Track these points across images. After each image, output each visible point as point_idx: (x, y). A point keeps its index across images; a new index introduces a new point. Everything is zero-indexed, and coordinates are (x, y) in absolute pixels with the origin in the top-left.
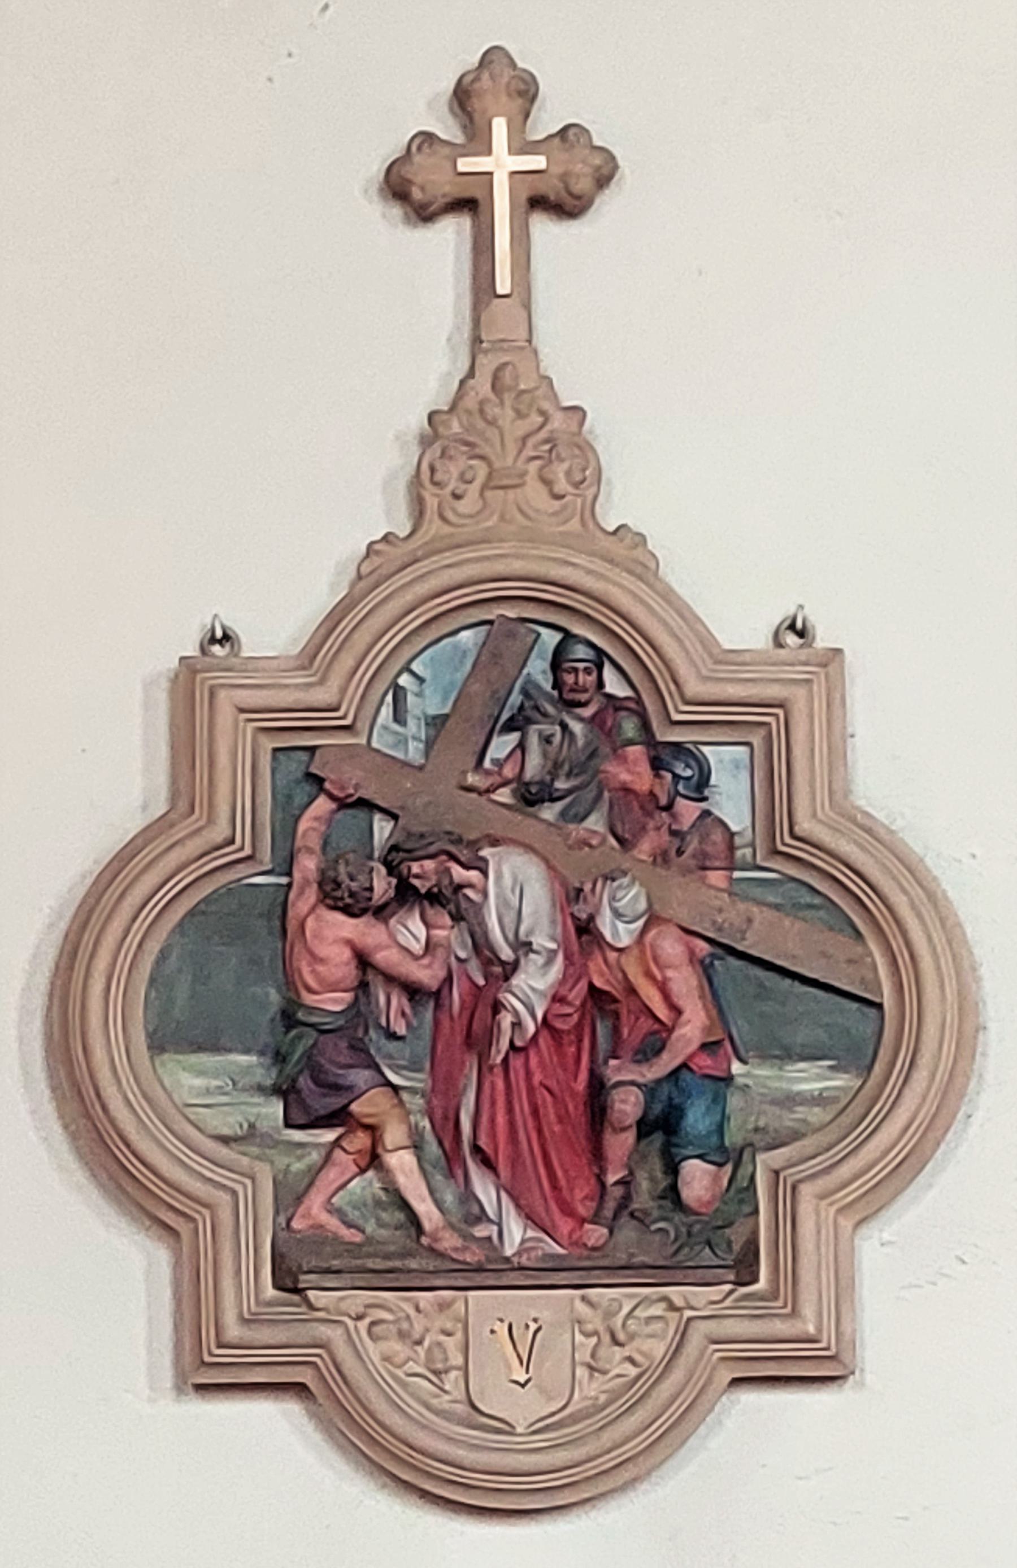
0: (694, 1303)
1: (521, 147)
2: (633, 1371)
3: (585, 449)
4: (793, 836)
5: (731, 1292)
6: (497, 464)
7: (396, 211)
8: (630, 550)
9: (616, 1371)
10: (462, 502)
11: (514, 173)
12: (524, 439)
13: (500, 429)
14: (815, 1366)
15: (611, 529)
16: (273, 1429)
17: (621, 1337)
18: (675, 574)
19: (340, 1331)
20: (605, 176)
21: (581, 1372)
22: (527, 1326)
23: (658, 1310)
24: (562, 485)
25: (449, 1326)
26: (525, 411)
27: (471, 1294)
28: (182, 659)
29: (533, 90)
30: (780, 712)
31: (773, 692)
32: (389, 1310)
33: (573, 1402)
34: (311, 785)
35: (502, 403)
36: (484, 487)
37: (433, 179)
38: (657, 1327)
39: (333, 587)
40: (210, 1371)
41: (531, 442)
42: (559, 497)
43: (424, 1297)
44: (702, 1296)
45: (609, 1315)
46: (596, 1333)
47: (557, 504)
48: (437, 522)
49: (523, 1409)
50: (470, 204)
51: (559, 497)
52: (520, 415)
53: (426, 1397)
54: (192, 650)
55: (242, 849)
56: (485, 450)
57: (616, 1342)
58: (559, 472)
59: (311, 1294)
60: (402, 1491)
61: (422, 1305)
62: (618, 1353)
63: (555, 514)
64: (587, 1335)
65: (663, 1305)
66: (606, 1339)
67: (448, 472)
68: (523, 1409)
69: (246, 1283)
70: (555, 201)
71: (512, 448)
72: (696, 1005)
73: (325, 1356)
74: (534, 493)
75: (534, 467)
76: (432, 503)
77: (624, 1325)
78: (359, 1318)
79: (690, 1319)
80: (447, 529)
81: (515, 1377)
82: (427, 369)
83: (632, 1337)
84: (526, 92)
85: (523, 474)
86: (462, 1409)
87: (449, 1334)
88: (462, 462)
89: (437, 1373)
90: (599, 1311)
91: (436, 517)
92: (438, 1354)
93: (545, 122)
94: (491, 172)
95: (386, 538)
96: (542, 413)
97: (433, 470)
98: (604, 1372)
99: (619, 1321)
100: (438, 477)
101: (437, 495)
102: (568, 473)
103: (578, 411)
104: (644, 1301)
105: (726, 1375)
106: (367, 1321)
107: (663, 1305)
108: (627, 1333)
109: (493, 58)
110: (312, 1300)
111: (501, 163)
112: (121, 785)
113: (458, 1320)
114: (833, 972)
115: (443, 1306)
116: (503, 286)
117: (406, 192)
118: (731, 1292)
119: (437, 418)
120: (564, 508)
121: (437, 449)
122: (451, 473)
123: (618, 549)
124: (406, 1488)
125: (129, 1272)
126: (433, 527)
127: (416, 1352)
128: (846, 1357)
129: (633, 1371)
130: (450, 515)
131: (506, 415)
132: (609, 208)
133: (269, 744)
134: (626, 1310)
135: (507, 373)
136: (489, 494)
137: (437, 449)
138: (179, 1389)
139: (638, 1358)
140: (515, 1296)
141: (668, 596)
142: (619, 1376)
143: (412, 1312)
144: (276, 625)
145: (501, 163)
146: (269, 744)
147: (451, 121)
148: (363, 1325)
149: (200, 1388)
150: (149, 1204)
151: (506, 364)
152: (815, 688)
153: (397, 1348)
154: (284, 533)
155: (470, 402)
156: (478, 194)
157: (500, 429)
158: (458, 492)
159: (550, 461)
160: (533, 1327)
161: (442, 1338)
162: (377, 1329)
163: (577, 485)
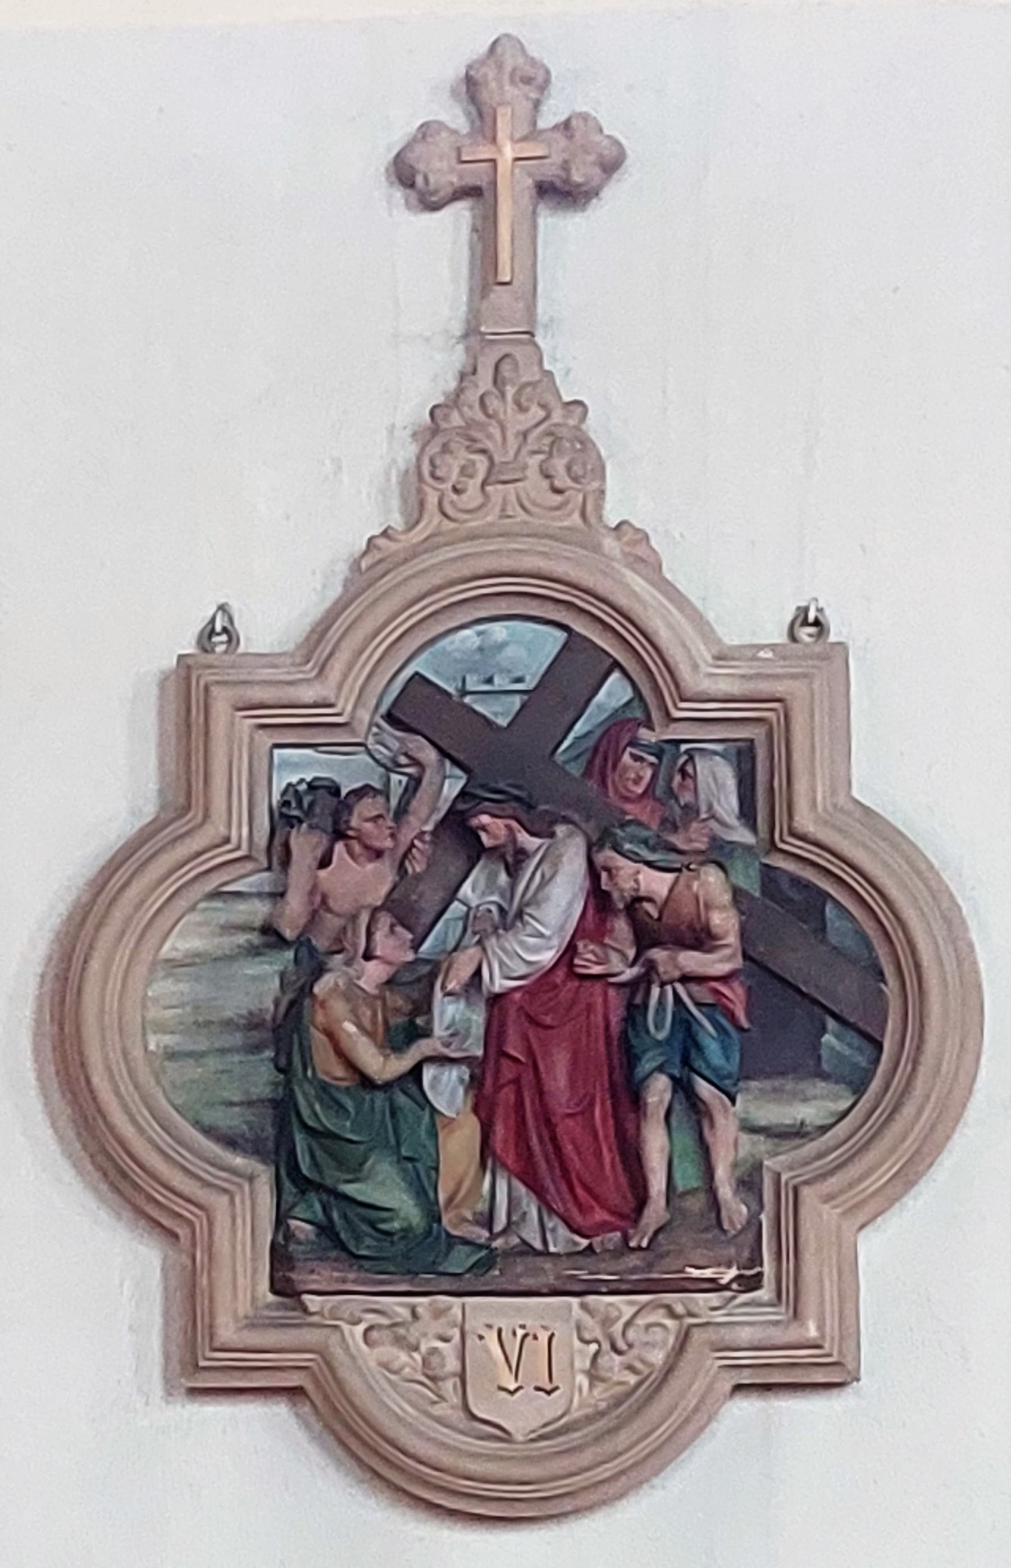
0: (695, 1310)
2: (632, 1379)
6: (497, 459)
7: (399, 194)
8: (638, 547)
10: (464, 497)
12: (525, 435)
13: (500, 421)
14: (822, 1373)
16: (259, 1434)
17: (621, 1345)
20: (611, 165)
22: (514, 1334)
24: (562, 480)
26: (525, 404)
28: (181, 657)
31: (778, 688)
34: (147, 1245)
35: (503, 395)
36: (484, 484)
38: (658, 1334)
42: (558, 491)
45: (607, 1322)
47: (558, 499)
48: (437, 518)
49: (524, 1415)
51: (558, 491)
54: (189, 647)
55: (238, 848)
56: (489, 445)
58: (559, 464)
59: (306, 1297)
60: (478, 1523)
61: (420, 1310)
63: (557, 508)
66: (606, 1346)
68: (524, 1415)
69: (242, 1279)
70: (560, 192)
71: (513, 443)
73: (320, 1360)
74: (534, 486)
76: (432, 500)
77: (624, 1334)
82: (425, 376)
83: (630, 1346)
84: (536, 81)
85: (525, 467)
86: (457, 1416)
87: (446, 1340)
88: (463, 456)
89: (433, 1379)
90: (597, 1319)
91: (436, 511)
92: (435, 1360)
94: (504, 164)
96: (543, 406)
97: (432, 463)
99: (619, 1327)
102: (569, 468)
106: (361, 1328)
112: (105, 785)
114: (824, 981)
115: (439, 1313)
119: (438, 411)
120: (566, 503)
122: (452, 468)
126: (432, 520)
127: (412, 1357)
128: (851, 1366)
129: (632, 1379)
130: (449, 510)
132: (616, 195)
137: (434, 448)
138: (169, 1391)
139: (639, 1365)
140: (506, 1304)
144: (271, 626)
146: (266, 739)
147: (458, 111)
149: (194, 1392)
150: (141, 1201)
151: (506, 356)
152: (816, 686)
154: (279, 530)
155: (472, 396)
157: (500, 421)
159: (550, 454)
160: (520, 1333)
161: (440, 1344)
162: (374, 1334)
163: (576, 479)
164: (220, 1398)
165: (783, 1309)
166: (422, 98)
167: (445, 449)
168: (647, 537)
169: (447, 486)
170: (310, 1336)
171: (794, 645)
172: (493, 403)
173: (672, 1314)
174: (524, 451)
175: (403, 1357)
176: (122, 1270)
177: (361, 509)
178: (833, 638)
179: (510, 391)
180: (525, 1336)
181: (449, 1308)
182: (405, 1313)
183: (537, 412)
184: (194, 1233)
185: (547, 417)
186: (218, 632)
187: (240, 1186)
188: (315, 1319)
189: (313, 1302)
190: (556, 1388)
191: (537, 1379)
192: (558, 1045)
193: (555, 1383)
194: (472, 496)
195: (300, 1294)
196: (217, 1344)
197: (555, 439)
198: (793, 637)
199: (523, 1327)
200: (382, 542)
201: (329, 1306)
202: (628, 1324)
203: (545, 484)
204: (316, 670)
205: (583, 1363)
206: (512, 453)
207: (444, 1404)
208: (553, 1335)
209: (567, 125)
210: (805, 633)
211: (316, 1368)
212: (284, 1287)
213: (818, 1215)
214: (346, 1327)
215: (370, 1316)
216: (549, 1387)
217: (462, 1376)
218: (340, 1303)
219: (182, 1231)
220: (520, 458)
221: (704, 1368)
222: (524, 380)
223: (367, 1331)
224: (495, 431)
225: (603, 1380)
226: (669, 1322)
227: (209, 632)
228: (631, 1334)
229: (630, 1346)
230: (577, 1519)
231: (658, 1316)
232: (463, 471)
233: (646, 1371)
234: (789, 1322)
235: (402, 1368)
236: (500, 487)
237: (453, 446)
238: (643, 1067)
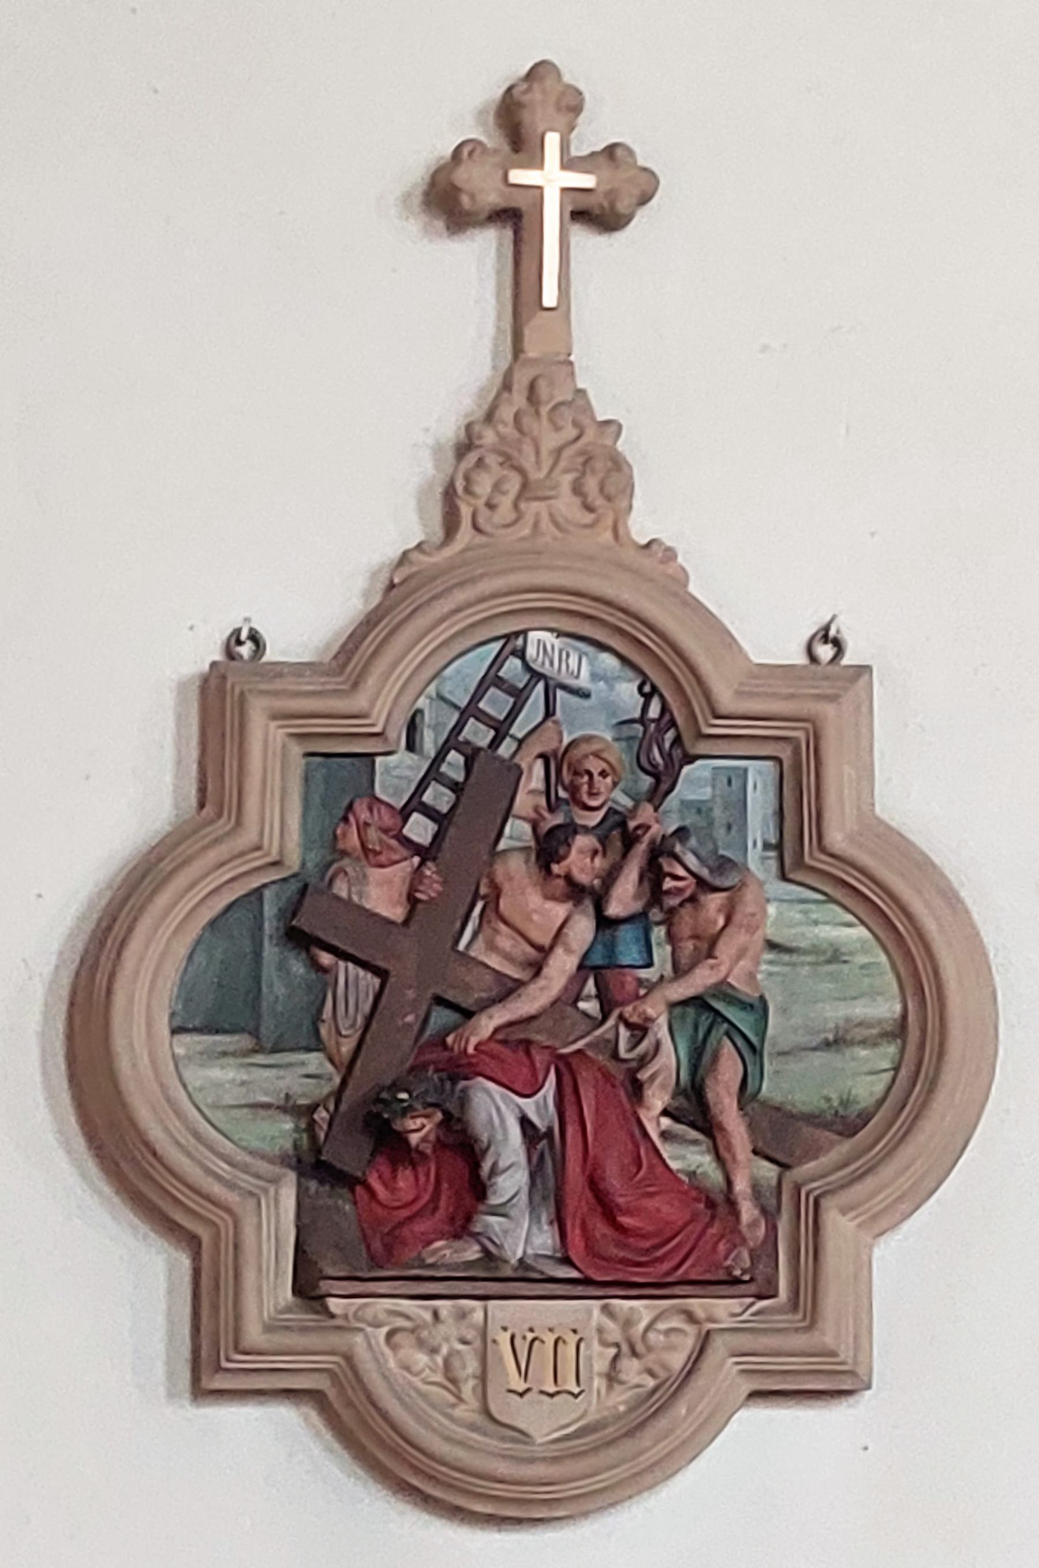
1: (568, 163)
2: (651, 1383)
3: (618, 464)
5: (752, 1304)
11: (564, 190)
12: (559, 452)
13: (530, 445)
14: (832, 1383)
17: (640, 1348)
27: (492, 1303)
32: (407, 1317)
35: (537, 413)
39: (366, 594)
41: (568, 453)
43: (444, 1306)
45: (628, 1324)
46: (617, 1345)
47: (589, 518)
50: (516, 218)
51: (589, 508)
57: (634, 1354)
58: (591, 484)
61: (444, 1313)
62: (635, 1364)
64: (604, 1343)
66: (625, 1348)
70: (595, 215)
71: (547, 463)
72: (72, 962)
73: (343, 1362)
74: (566, 505)
75: (569, 478)
78: (378, 1325)
80: (480, 539)
81: (513, 1387)
84: (572, 105)
86: (479, 1419)
92: (456, 1363)
93: (590, 138)
94: (514, 182)
95: (419, 547)
97: (467, 478)
105: (748, 1386)
106: (385, 1330)
109: (540, 71)
112: (127, 789)
116: (550, 297)
117: (445, 202)
121: (472, 458)
123: (646, 562)
125: (137, 1278)
128: (861, 1370)
139: (657, 1369)
141: (696, 606)
145: (551, 180)
155: (506, 413)
157: (530, 445)
159: (583, 474)
162: (398, 1338)
163: (609, 498)
164: (811, 1398)
165: (799, 1316)
166: (450, 117)
169: (481, 502)
170: (335, 1340)
171: (813, 667)
172: (527, 421)
173: (691, 1317)
174: (557, 471)
175: (422, 1359)
177: (393, 522)
179: (544, 410)
180: (512, 1338)
181: (473, 1310)
182: (428, 1316)
183: (571, 432)
184: (218, 1232)
185: (578, 438)
186: (244, 644)
187: (266, 1191)
188: (338, 1322)
189: (334, 1304)
190: (580, 1393)
191: (508, 1383)
193: (582, 1387)
195: (322, 1297)
196: (241, 1347)
197: (588, 460)
198: (813, 658)
199: (531, 1330)
200: (416, 556)
201: (353, 1309)
202: (649, 1328)
203: (577, 501)
204: (350, 683)
205: (601, 1365)
206: (545, 471)
207: (463, 1407)
208: (581, 1340)
210: (825, 652)
212: (307, 1288)
213: (838, 1225)
214: (369, 1329)
215: (392, 1319)
216: (576, 1390)
218: (366, 1305)
220: (553, 475)
221: (723, 1370)
222: (559, 399)
223: (390, 1335)
224: (528, 449)
225: (622, 1383)
226: (691, 1329)
229: (650, 1349)
232: (497, 487)
233: (663, 1375)
234: (264, 1322)
235: (422, 1371)
237: (487, 461)
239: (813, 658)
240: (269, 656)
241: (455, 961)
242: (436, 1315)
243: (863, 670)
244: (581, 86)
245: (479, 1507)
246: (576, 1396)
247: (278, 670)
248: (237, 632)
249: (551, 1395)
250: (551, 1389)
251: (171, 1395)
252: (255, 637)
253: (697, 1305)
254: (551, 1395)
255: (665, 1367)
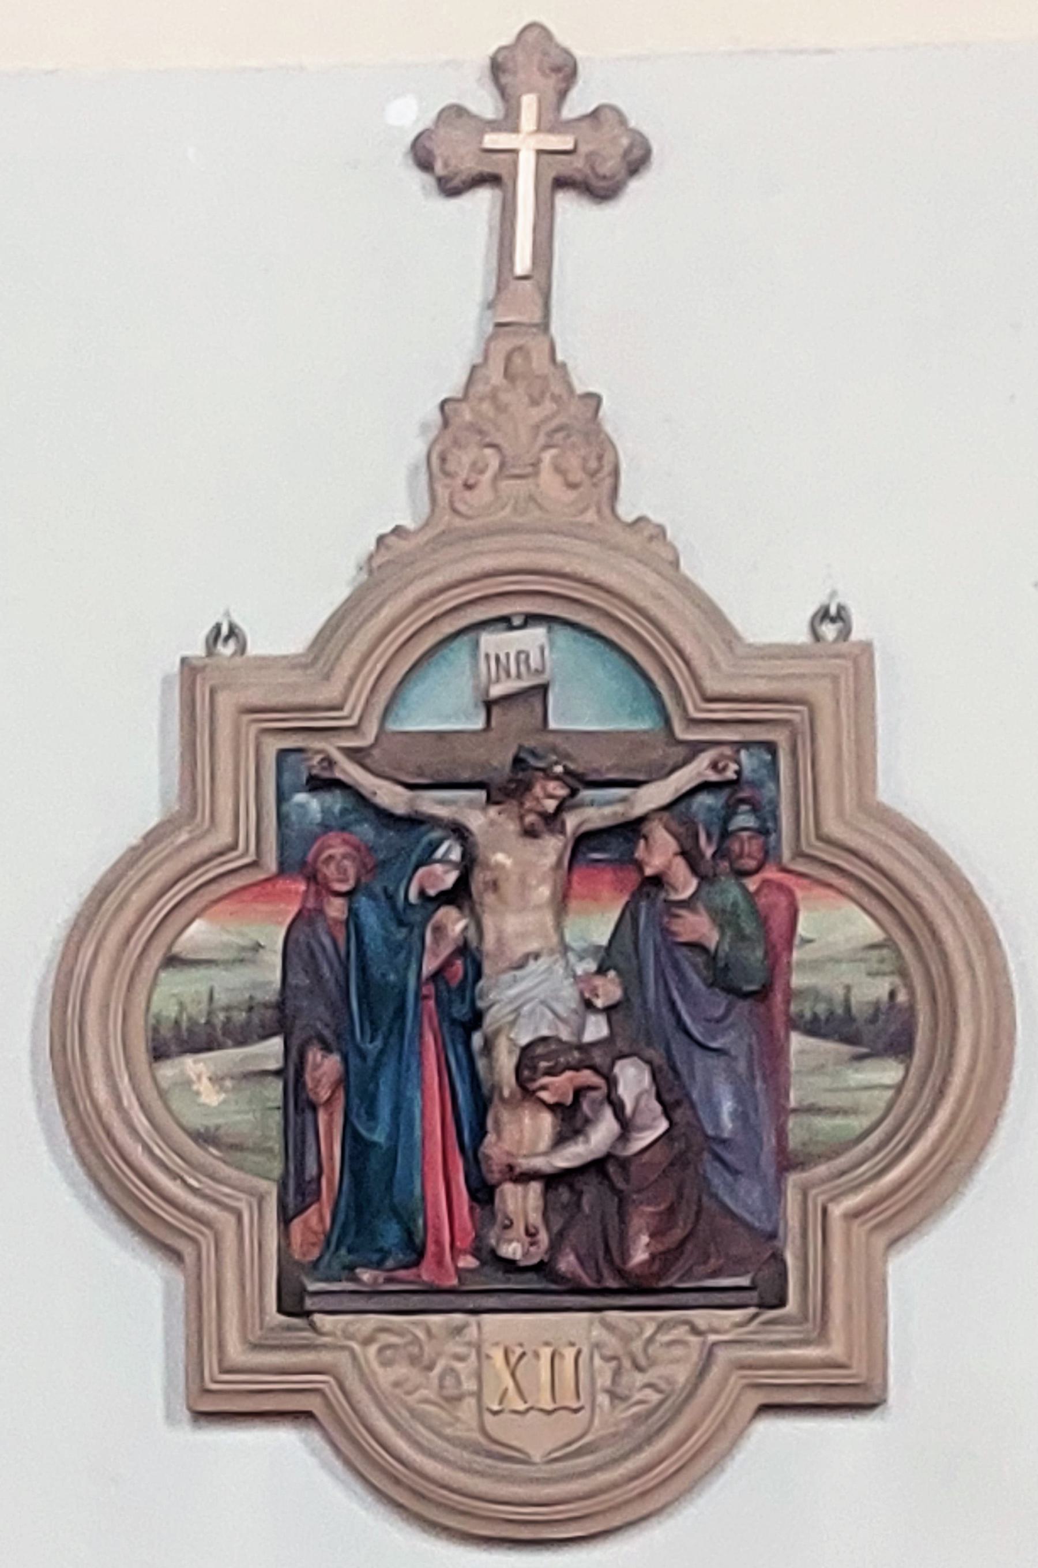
1: (509, 122)
2: (655, 1397)
4: (820, 837)
5: (755, 1316)
6: (509, 451)
9: (638, 1396)
10: (476, 492)
11: (540, 152)
12: (537, 427)
13: (520, 416)
14: (854, 1396)
15: (630, 518)
16: (284, 1451)
17: (642, 1361)
18: (703, 570)
19: (344, 1357)
20: (637, 160)
21: (603, 1399)
23: (681, 1332)
25: (461, 1350)
27: (486, 1317)
29: (571, 64)
30: (803, 708)
33: (593, 1430)
36: (495, 479)
37: (458, 155)
38: (678, 1351)
40: (215, 1405)
44: (727, 1319)
47: (572, 495)
49: (538, 1438)
51: (572, 486)
52: (535, 402)
53: (436, 1423)
54: (197, 650)
56: (498, 440)
59: (317, 1318)
60: (485, 1546)
62: (640, 1379)
65: (687, 1328)
66: (627, 1364)
67: (460, 463)
68: (538, 1438)
70: (599, 189)
77: (645, 1350)
78: (367, 1341)
79: (715, 1344)
80: (458, 522)
82: (444, 342)
83: (653, 1362)
84: (566, 72)
85: (536, 464)
87: (460, 1358)
92: (449, 1381)
97: (443, 460)
98: (624, 1399)
99: (637, 1346)
100: (451, 466)
101: (447, 486)
103: (594, 400)
104: (661, 1327)
107: (687, 1328)
108: (648, 1358)
109: (535, 35)
110: (319, 1324)
111: (526, 144)
112: (109, 783)
113: (469, 1344)
118: (755, 1316)
122: (462, 461)
124: (511, 1545)
129: (655, 1397)
130: (462, 507)
131: (515, 398)
133: (272, 746)
134: (648, 1332)
135: (518, 360)
136: (504, 484)
142: (641, 1402)
143: (421, 1335)
144: (282, 629)
145: (526, 144)
148: (373, 1349)
149: (203, 1417)
151: (520, 348)
153: (401, 1370)
156: (504, 172)
157: (520, 416)
158: (471, 481)
163: (593, 474)
167: (456, 443)
168: (662, 531)
169: (459, 482)
171: (819, 645)
173: (695, 1331)
176: (141, 1289)
178: (855, 636)
180: (523, 1354)
192: (606, 1054)
194: (483, 494)
196: (226, 1364)
198: (817, 637)
199: (521, 1345)
200: (392, 540)
201: (340, 1326)
202: (651, 1340)
203: (558, 479)
205: (604, 1380)
209: (595, 114)
210: (829, 631)
211: (327, 1391)
216: (575, 1405)
217: (479, 1395)
219: (187, 1250)
223: (381, 1350)
226: (694, 1339)
227: (215, 636)
228: (651, 1350)
230: (660, 1523)
231: (681, 1332)
236: (512, 482)
238: (218, 1111)
239: (817, 637)
240: (252, 650)
241: (892, 995)
242: (429, 1332)
243: (867, 647)
244: (578, 53)
245: (617, 1520)
246: (576, 1411)
247: (265, 663)
248: (218, 628)
249: (549, 1413)
250: (550, 1406)
251: (170, 1417)
252: (233, 632)
253: (701, 1317)
254: (549, 1413)
255: (670, 1381)
